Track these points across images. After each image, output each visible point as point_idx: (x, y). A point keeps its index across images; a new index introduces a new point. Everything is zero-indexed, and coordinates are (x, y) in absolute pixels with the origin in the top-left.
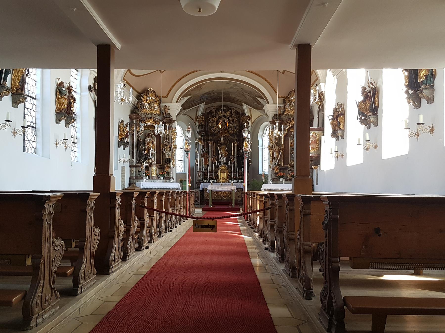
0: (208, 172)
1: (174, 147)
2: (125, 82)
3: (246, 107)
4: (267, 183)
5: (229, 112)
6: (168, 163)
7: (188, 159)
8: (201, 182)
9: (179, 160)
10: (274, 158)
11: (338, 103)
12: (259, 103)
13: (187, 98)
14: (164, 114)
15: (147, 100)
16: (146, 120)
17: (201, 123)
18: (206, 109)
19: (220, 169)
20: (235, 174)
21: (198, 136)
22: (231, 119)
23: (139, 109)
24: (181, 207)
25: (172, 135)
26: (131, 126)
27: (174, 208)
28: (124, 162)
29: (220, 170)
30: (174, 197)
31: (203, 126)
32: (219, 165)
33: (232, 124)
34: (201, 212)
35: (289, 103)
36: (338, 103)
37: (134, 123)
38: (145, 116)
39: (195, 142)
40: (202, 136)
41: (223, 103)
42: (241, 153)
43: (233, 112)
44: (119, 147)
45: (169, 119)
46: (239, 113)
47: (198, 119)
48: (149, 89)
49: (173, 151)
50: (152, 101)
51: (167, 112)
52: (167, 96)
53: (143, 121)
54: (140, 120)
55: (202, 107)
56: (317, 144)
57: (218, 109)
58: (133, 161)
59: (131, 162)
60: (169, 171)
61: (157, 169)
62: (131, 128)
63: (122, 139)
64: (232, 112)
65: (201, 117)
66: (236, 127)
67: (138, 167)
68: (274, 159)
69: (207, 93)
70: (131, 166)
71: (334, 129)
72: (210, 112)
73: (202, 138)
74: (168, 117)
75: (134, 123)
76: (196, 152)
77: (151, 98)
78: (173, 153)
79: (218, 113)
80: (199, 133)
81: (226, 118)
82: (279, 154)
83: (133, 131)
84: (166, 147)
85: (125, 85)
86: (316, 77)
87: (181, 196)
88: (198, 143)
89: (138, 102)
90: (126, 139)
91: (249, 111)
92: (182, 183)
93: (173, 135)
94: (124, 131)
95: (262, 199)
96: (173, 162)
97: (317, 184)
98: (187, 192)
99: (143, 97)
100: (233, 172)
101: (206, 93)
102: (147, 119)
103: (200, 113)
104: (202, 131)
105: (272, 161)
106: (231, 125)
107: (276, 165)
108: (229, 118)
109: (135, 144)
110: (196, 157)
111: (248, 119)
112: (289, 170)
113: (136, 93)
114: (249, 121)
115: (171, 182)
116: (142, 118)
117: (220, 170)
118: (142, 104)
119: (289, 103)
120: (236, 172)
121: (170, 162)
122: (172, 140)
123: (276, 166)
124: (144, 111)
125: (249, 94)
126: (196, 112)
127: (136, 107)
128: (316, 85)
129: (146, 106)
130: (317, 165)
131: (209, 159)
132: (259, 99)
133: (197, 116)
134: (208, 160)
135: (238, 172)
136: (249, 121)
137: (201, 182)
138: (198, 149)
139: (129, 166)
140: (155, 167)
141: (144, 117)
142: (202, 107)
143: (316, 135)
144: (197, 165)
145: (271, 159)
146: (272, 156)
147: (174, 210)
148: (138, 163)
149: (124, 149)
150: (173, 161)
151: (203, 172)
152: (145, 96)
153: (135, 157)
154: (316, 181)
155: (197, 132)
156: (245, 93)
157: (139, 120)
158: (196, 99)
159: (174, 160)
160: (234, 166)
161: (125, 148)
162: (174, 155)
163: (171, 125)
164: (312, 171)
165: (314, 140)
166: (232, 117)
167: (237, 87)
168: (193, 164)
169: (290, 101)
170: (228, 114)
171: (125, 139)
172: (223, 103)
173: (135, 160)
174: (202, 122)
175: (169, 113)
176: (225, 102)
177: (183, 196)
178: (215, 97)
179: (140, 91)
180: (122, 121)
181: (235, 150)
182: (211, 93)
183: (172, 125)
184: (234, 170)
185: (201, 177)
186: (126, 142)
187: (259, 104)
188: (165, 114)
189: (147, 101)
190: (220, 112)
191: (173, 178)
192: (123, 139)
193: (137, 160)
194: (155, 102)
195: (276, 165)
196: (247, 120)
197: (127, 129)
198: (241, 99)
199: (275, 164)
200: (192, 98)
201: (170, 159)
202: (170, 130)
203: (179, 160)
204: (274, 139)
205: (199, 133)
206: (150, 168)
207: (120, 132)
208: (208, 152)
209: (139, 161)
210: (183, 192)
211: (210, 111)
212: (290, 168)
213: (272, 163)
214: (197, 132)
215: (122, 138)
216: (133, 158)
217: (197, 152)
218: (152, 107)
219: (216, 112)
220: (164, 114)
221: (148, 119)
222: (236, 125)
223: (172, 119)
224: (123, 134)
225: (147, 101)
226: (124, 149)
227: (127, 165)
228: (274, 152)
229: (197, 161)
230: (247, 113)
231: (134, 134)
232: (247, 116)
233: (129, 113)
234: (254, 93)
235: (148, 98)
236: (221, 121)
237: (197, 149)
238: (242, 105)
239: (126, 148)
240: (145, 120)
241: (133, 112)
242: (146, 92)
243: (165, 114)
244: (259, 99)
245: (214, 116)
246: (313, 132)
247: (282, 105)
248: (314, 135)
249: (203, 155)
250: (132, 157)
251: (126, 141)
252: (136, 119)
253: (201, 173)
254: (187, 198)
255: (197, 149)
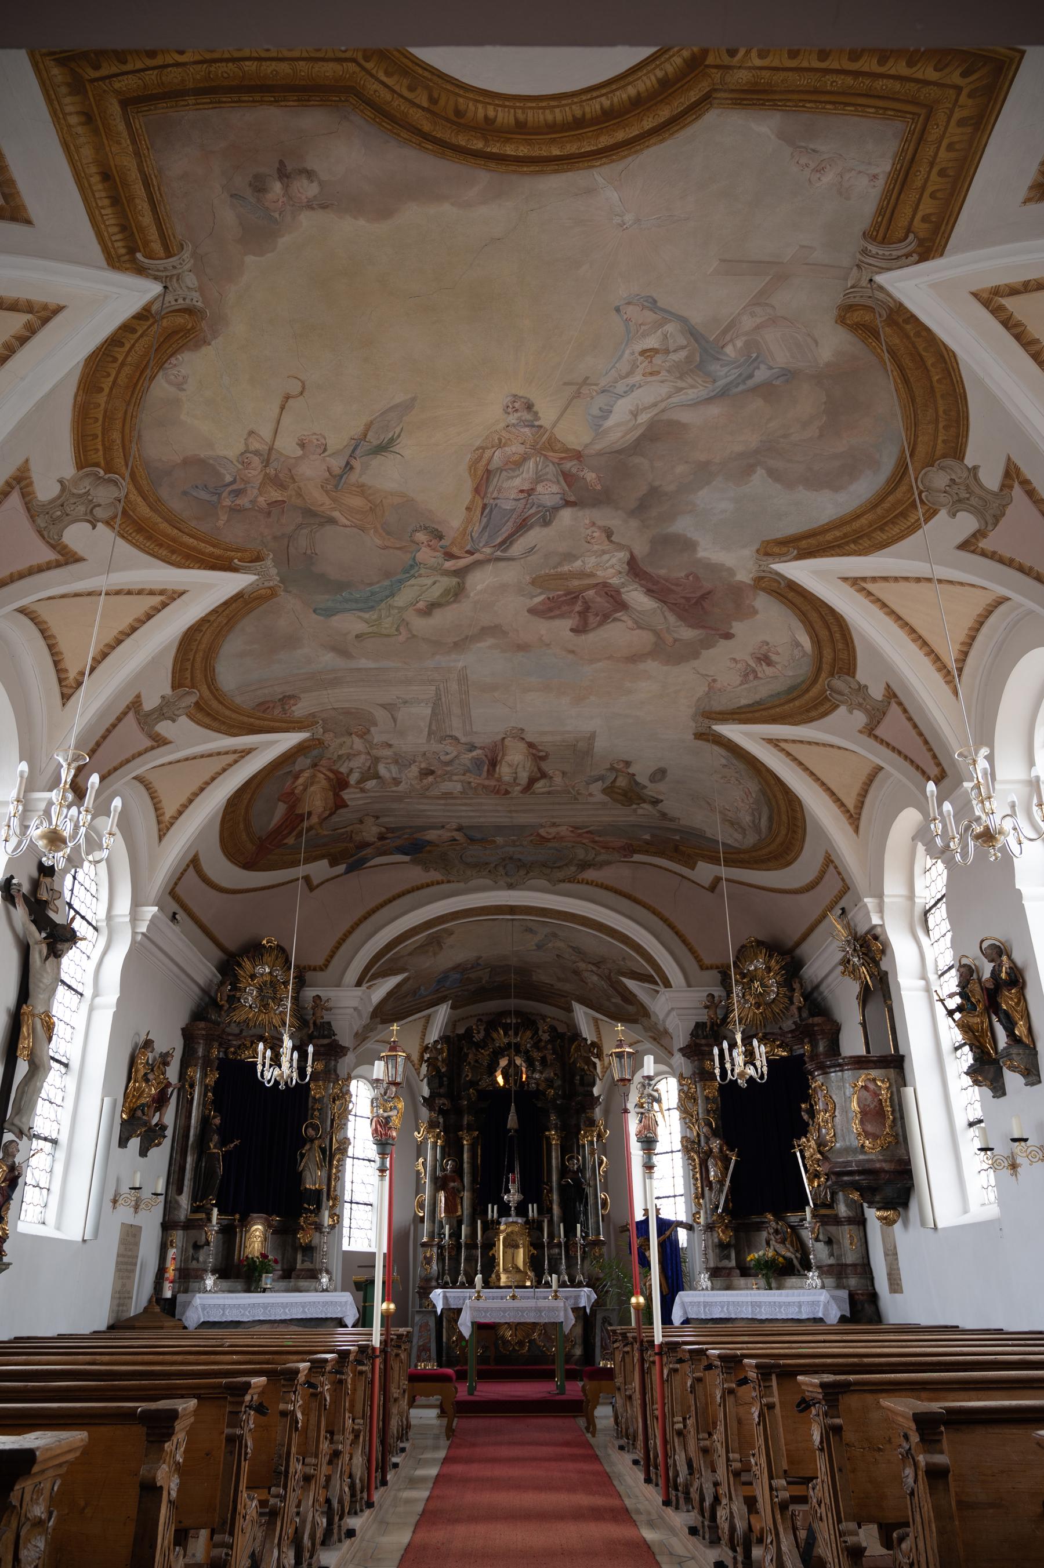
0: (460, 1244)
1: (338, 1149)
2: (175, 907)
3: (583, 1018)
4: (695, 1289)
5: (529, 1034)
6: (311, 1212)
7: (387, 1178)
8: (434, 1283)
9: (357, 1203)
10: (710, 1182)
11: (982, 941)
12: (629, 997)
13: (392, 982)
14: (311, 1025)
15: (253, 977)
16: (245, 1045)
17: (438, 1071)
18: (452, 1023)
19: (503, 1232)
20: (557, 1251)
21: (425, 1113)
22: (536, 1055)
23: (223, 1006)
24: (340, 1447)
25: (334, 1102)
26: (187, 1068)
27: (285, 1488)
28: (136, 1208)
29: (501, 1238)
30: (291, 1407)
31: (445, 1079)
32: (500, 1215)
33: (541, 1073)
34: (435, 1422)
35: (743, 984)
36: (982, 941)
37: (200, 1053)
38: (241, 1031)
39: (416, 1133)
40: (441, 1112)
41: (512, 1003)
42: (574, 1172)
43: (544, 1032)
44: (123, 1143)
45: (326, 1041)
46: (562, 1036)
47: (426, 1056)
48: (264, 942)
49: (335, 1162)
50: (271, 982)
51: (322, 1017)
52: (326, 966)
53: (232, 1049)
54: (220, 1045)
55: (442, 1014)
56: (888, 1123)
57: (493, 1022)
58: (177, 1202)
59: (170, 1207)
60: (313, 1244)
61: (269, 1234)
62: (186, 1073)
63: (135, 1110)
64: (540, 1032)
65: (436, 1049)
66: (552, 1082)
67: (194, 1227)
68: (711, 1189)
69: (459, 965)
70: (167, 1226)
71: (978, 1048)
72: (466, 1031)
73: (441, 1120)
74: (324, 1037)
75: (200, 1053)
76: (418, 1173)
77: (267, 970)
78: (334, 1171)
79: (495, 1035)
80: (428, 1102)
81: (518, 1052)
82: (727, 1169)
83: (192, 1086)
84: (307, 1147)
85: (177, 916)
86: (841, 883)
87: (341, 1381)
88: (426, 1139)
89: (222, 983)
90: (158, 1114)
91: (593, 1029)
92: (361, 1293)
93: (337, 1102)
94: (147, 1081)
95: (770, 1400)
96: (334, 1205)
97: (895, 1286)
98: (374, 1349)
99: (240, 965)
100: (548, 1243)
101: (454, 969)
102: (248, 1044)
103: (434, 1035)
104: (440, 1096)
105: (703, 1196)
106: (537, 1076)
107: (720, 1211)
108: (528, 1051)
109: (195, 1135)
110: (419, 1189)
111: (593, 1054)
112: (771, 1231)
113: (218, 954)
114: (596, 1060)
115: (323, 1291)
116: (230, 1038)
117: (501, 1238)
118: (235, 988)
119: (743, 984)
120: (559, 1245)
121: (319, 1208)
122: (332, 1121)
123: (720, 1216)
124: (239, 1016)
125: (594, 969)
126: (420, 1035)
127: (214, 1003)
128: (840, 912)
129: (250, 997)
130: (894, 1209)
131: (462, 1198)
132: (631, 984)
133: (426, 1042)
134: (459, 1201)
135: (566, 1243)
136: (596, 1060)
137: (434, 1283)
138: (426, 1160)
139: (162, 1224)
140: (260, 1227)
141: (235, 1035)
142: (442, 1014)
143: (879, 1083)
144: (422, 1219)
145: (697, 1189)
146: (698, 1176)
147: (283, 1498)
148: (195, 1210)
149: (143, 1153)
150: (331, 1203)
151: (440, 1247)
152: (247, 964)
153: (185, 1189)
154: (889, 1275)
155: (423, 1097)
156: (582, 965)
157: (216, 1045)
158: (422, 988)
159: (335, 1199)
160: (551, 1222)
161: (148, 1150)
162: (337, 1178)
163: (333, 1063)
164: (862, 1234)
165: (872, 1106)
166: (539, 1049)
167: (560, 944)
168: (404, 1218)
169: (744, 976)
170: (525, 1039)
171: (155, 1112)
172: (512, 1003)
173: (184, 1200)
174: (439, 1064)
175: (329, 1023)
176: (517, 1001)
177: (349, 1381)
178: (484, 982)
179: (232, 945)
180: (148, 1044)
181: (554, 1161)
182: (472, 968)
183: (335, 1066)
184: (551, 1236)
185: (435, 1267)
186: (156, 1125)
187: (631, 1003)
188: (315, 1023)
189: (252, 980)
190: (502, 1032)
191: (328, 1272)
192: (139, 1113)
193: (194, 1198)
194: (283, 983)
195: (720, 1211)
196: (589, 1058)
197: (164, 1073)
198: (567, 987)
199: (717, 1207)
200: (411, 981)
201: (319, 1192)
202: (329, 1082)
203: (357, 1203)
204: (700, 1111)
205: (428, 1102)
206: (241, 1231)
207: (131, 1084)
208: (458, 1171)
209: (201, 1201)
210: (352, 1357)
211: (469, 1030)
212: (773, 1224)
213: (700, 1204)
214: (423, 1097)
215: (138, 1107)
216: (180, 1192)
217: (423, 1170)
218: (270, 1001)
219: (488, 1034)
220: (311, 1025)
221: (252, 1043)
222: (555, 1074)
223: (335, 1040)
224: (144, 1091)
225: (252, 980)
226: (143, 1153)
227: (150, 1221)
228: (707, 1160)
229: (421, 1206)
230: (587, 1032)
231: (192, 1099)
232: (589, 1042)
233: (182, 1019)
234: (614, 962)
235: (259, 970)
236: (503, 1062)
237: (421, 1160)
238: (570, 1010)
239: (153, 1152)
240: (239, 1047)
241: (198, 1015)
242: (254, 950)
243: (315, 1023)
244: (631, 984)
245: (478, 1046)
246: (866, 1071)
247: (718, 992)
248: (871, 1086)
249: (440, 1183)
250: (175, 1188)
251: (154, 1121)
252: (209, 1040)
253: (435, 1249)
254: (372, 1382)
255: (421, 1160)
